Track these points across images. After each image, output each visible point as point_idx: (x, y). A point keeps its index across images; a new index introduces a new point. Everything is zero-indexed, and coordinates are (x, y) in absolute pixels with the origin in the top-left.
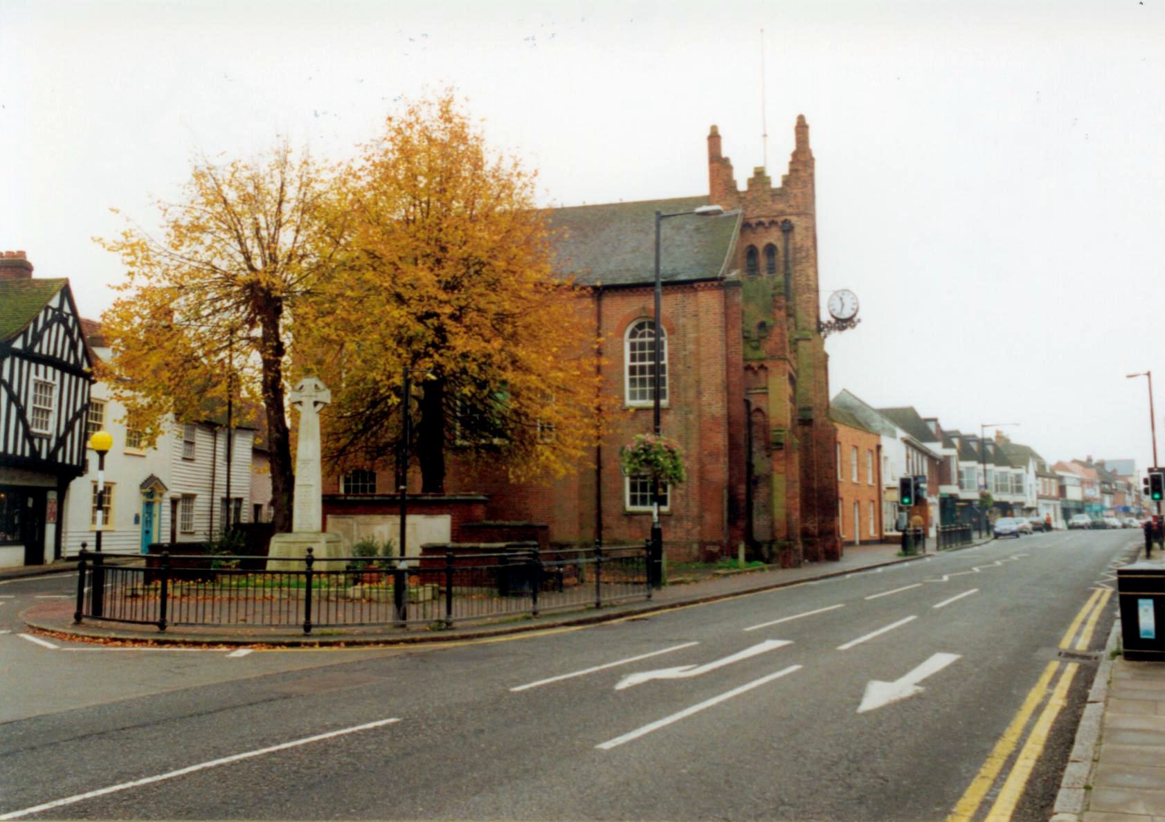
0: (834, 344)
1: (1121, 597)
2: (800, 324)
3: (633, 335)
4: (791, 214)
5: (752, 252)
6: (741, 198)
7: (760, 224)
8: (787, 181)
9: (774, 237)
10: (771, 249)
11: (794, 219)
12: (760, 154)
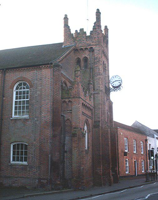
0: (114, 96)
1: (24, 161)
2: (96, 88)
3: (17, 89)
4: (93, 45)
5: (78, 61)
7: (82, 49)
9: (87, 54)
10: (86, 59)
11: (94, 47)
12: (83, 23)
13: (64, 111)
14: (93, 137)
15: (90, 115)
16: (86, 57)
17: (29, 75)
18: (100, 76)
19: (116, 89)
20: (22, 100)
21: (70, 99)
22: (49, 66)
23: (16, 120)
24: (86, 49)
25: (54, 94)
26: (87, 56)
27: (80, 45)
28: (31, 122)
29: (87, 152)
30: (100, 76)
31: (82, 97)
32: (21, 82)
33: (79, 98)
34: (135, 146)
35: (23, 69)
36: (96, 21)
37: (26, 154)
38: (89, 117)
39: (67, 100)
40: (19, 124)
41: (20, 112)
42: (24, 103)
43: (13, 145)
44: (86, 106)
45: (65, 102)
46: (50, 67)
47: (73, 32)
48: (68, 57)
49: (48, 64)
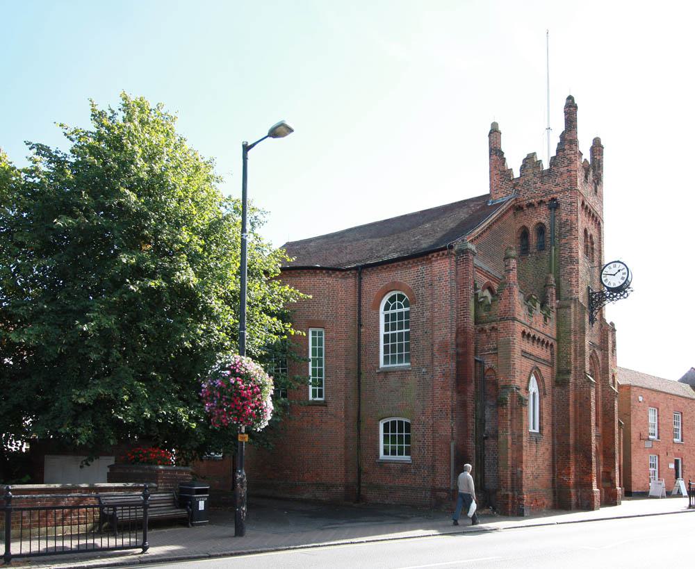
3: (387, 308)
4: (557, 192)
6: (516, 184)
7: (530, 205)
8: (554, 161)
9: (543, 216)
10: (541, 229)
11: (559, 196)
12: (531, 140)
13: (482, 351)
14: (553, 406)
15: (546, 359)
16: (540, 223)
17: (407, 276)
18: (573, 267)
19: (615, 294)
20: (397, 331)
21: (494, 324)
22: (446, 252)
23: (386, 373)
24: (541, 203)
25: (457, 316)
26: (543, 221)
27: (528, 194)
28: (415, 376)
29: (536, 439)
30: (573, 267)
31: (522, 320)
32: (392, 293)
33: (514, 319)
34: (680, 428)
35: (395, 264)
36: (564, 130)
37: (408, 440)
38: (544, 362)
39: (487, 327)
40: (393, 380)
41: (393, 357)
42: (400, 339)
43: (384, 424)
44: (534, 337)
45: (482, 331)
46: (449, 255)
47: (514, 164)
48: (495, 227)
49: (444, 249)
